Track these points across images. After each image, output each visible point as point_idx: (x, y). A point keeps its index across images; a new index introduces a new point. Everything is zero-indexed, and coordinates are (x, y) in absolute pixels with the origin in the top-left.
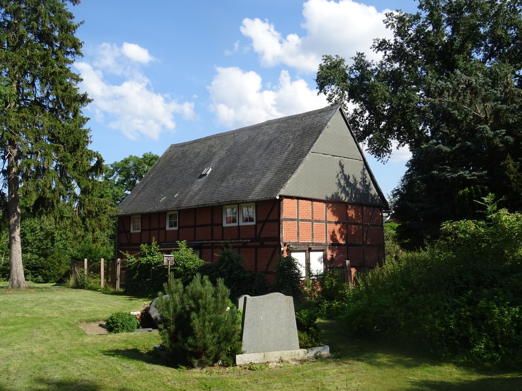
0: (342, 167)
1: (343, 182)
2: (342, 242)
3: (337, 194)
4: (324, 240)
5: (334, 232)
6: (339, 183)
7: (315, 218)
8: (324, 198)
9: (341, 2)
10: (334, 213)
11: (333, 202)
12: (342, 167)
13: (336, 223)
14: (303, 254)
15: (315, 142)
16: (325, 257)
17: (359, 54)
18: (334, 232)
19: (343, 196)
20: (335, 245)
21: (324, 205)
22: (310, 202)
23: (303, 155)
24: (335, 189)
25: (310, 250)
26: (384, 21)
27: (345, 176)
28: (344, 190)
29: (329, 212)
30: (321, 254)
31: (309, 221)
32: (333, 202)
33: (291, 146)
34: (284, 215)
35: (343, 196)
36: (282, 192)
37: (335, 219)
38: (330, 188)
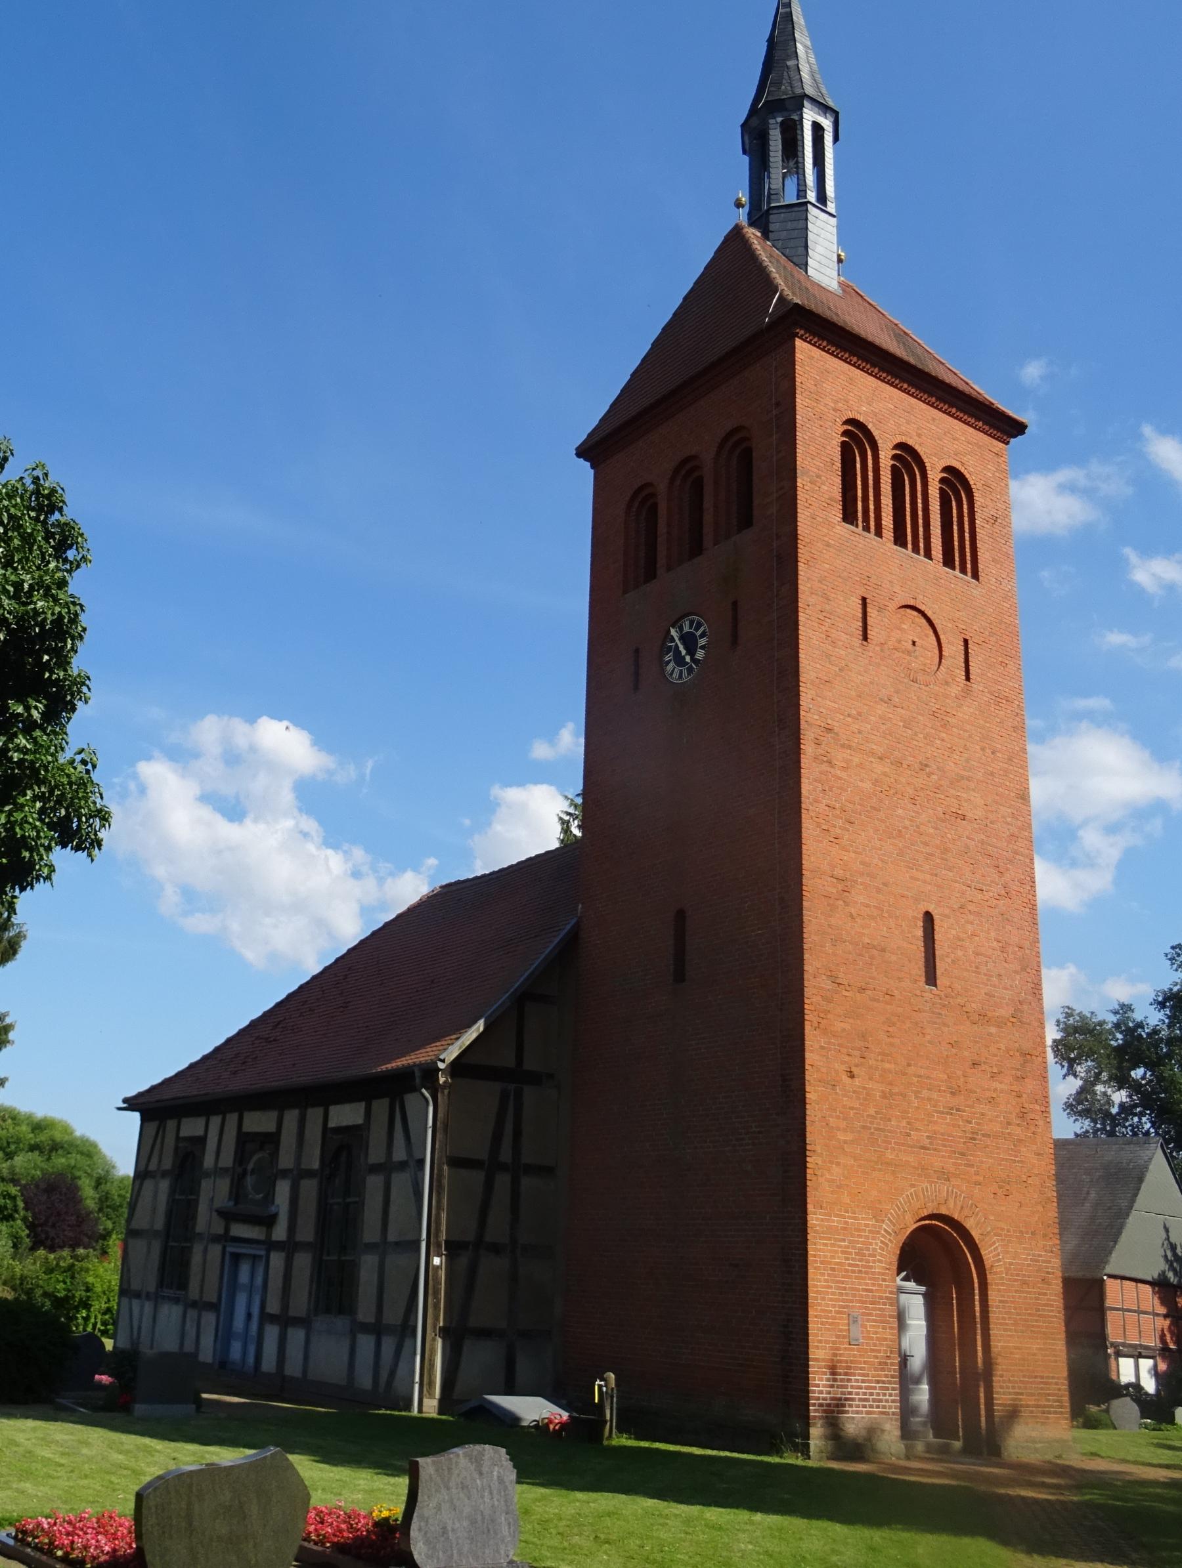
0: (1167, 1231)
1: (1169, 1254)
2: (1172, 1347)
3: (1164, 1272)
4: (1153, 1342)
5: (1163, 1330)
6: (1166, 1256)
7: (1142, 1308)
8: (1150, 1279)
9: (585, 471)
10: (1163, 1302)
11: (1160, 1285)
12: (1167, 1231)
13: (1165, 1316)
14: (1131, 1361)
15: (1136, 1195)
16: (1155, 1366)
17: (1123, 1006)
18: (1163, 1330)
19: (1170, 1275)
20: (1165, 1351)
21: (1148, 1288)
22: (1134, 1284)
23: (1124, 1214)
24: (1162, 1266)
25: (1140, 1356)
26: (1166, 955)
27: (1171, 1244)
28: (1172, 1268)
29: (1157, 1302)
30: (1150, 1362)
31: (1135, 1311)
32: (1160, 1285)
33: (1093, 1195)
34: (1109, 1303)
35: (1170, 1275)
36: (1109, 1269)
37: (1162, 1310)
38: (1155, 1266)
